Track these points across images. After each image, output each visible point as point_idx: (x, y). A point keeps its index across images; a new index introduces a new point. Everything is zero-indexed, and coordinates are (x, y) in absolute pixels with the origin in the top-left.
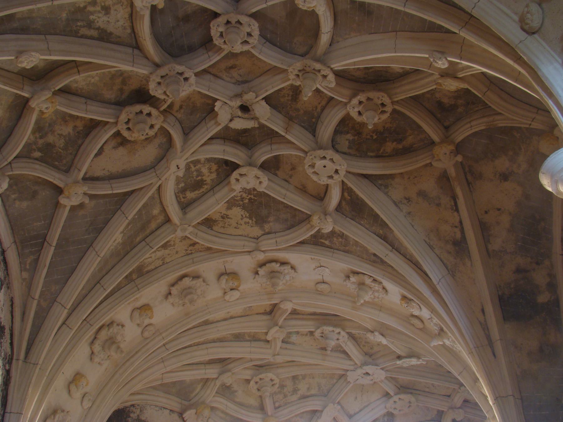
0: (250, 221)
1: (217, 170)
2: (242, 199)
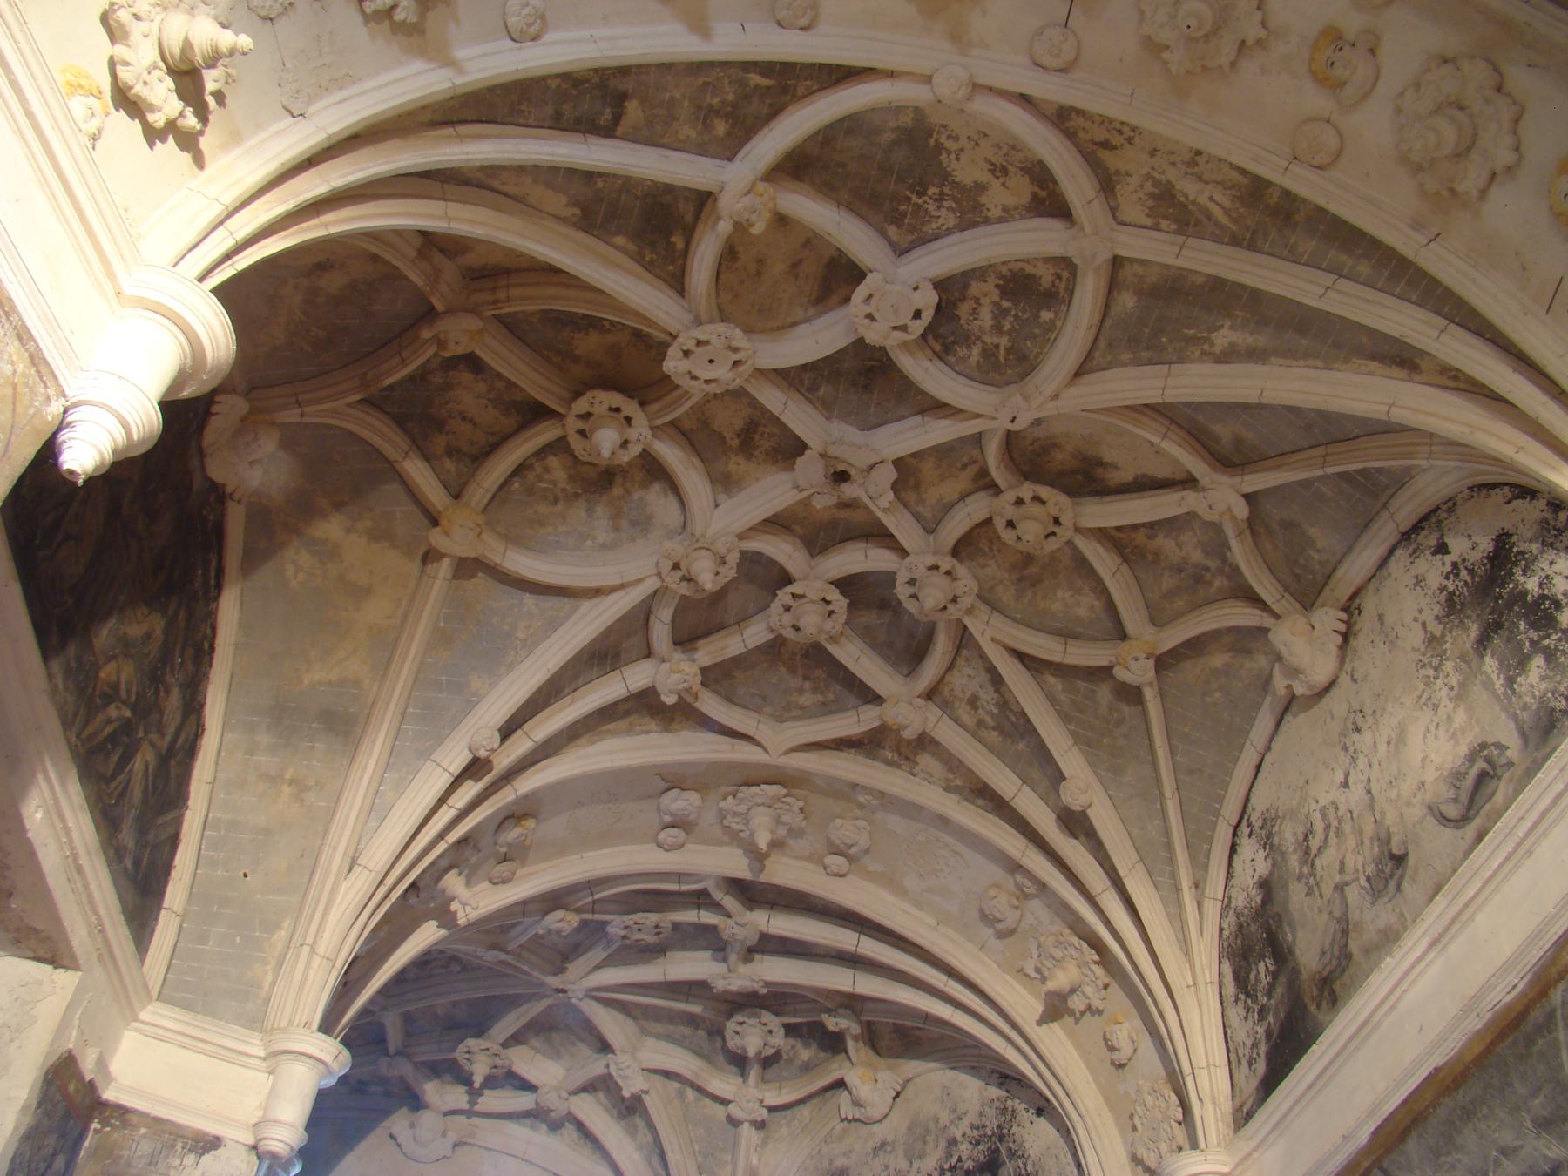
0: (943, 139)
1: (963, 299)
2: (940, 199)
